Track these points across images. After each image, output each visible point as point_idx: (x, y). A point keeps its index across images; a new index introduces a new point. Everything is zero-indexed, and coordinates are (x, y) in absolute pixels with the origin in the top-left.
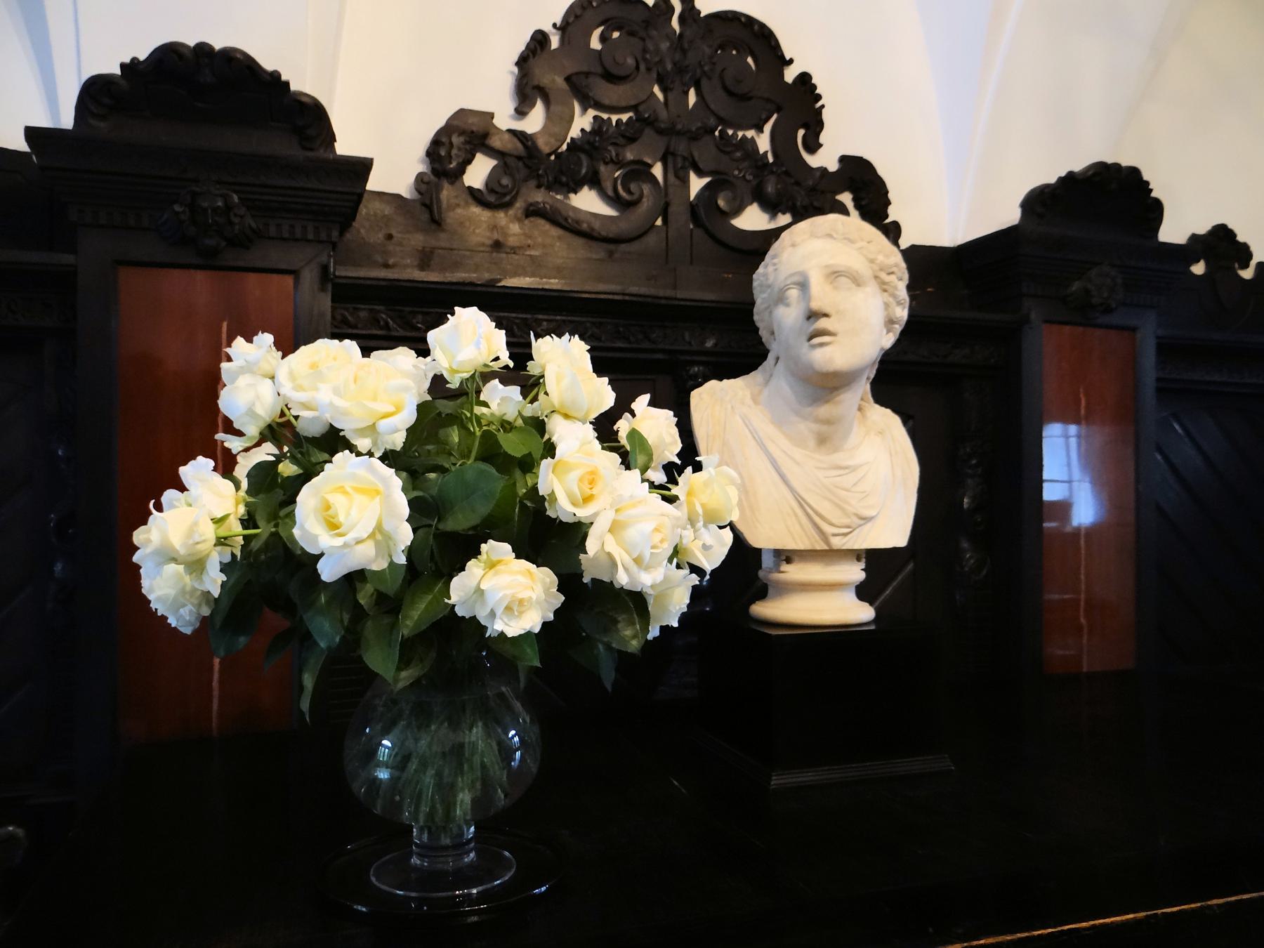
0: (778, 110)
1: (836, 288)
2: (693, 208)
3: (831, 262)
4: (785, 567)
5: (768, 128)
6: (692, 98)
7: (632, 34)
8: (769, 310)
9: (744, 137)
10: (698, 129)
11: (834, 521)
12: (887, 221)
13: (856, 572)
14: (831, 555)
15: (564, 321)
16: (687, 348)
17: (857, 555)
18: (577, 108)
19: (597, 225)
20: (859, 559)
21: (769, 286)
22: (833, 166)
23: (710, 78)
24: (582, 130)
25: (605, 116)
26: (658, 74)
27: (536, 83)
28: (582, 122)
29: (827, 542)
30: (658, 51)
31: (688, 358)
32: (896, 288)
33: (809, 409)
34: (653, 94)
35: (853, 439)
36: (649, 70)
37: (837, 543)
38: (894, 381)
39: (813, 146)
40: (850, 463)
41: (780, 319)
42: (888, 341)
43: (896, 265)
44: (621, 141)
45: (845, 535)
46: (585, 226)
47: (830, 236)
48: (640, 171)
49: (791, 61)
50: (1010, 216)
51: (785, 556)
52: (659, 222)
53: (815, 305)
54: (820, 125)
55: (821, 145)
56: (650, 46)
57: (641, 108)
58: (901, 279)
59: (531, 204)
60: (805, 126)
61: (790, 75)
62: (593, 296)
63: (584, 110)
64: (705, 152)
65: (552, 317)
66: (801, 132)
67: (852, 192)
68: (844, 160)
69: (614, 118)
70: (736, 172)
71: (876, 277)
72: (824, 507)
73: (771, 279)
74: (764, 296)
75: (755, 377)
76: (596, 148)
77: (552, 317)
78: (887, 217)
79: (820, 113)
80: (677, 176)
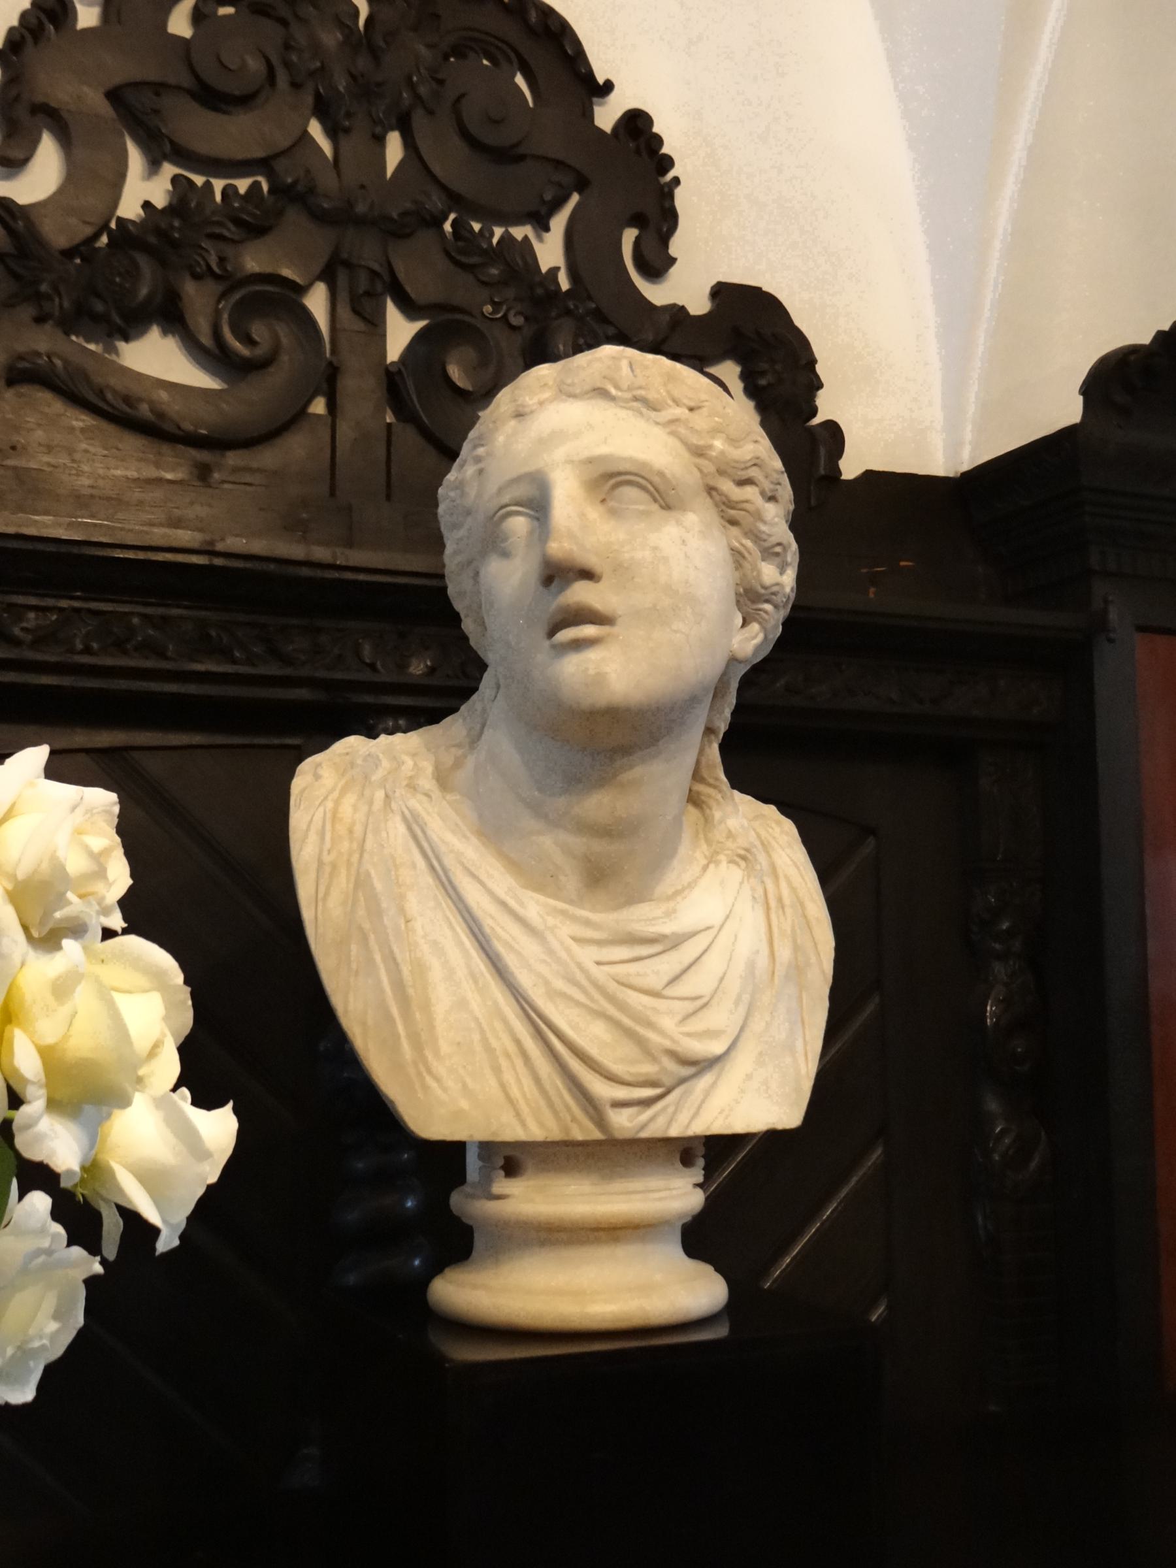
0: (582, 185)
1: (613, 513)
2: (393, 382)
3: (603, 450)
4: (502, 1185)
5: (559, 223)
6: (394, 150)
7: (261, 11)
8: (473, 567)
9: (507, 239)
10: (404, 214)
11: (618, 1069)
12: (816, 421)
13: (680, 1194)
14: (612, 1155)
15: (77, 610)
16: (367, 676)
17: (685, 1151)
18: (135, 159)
19: (174, 407)
20: (687, 1160)
21: (468, 512)
22: (699, 305)
23: (431, 112)
24: (147, 205)
25: (199, 180)
26: (318, 97)
27: (40, 99)
28: (143, 189)
29: (600, 1121)
30: (316, 48)
31: (369, 699)
32: (758, 516)
33: (561, 802)
34: (305, 136)
35: (679, 872)
36: (296, 85)
37: (624, 1122)
38: (777, 733)
39: (656, 265)
40: (667, 928)
41: (497, 590)
42: (750, 641)
43: (757, 463)
44: (230, 231)
45: (647, 1103)
46: (144, 410)
47: (601, 393)
48: (283, 298)
49: (608, 87)
50: (1066, 409)
51: (510, 1159)
52: (319, 407)
53: (558, 547)
54: (669, 219)
55: (673, 261)
56: (300, 36)
57: (280, 165)
58: (772, 499)
59: (21, 358)
60: (638, 220)
61: (606, 116)
62: (141, 556)
63: (154, 165)
64: (421, 267)
65: (50, 602)
66: (629, 236)
67: (740, 359)
68: (720, 291)
69: (218, 185)
70: (488, 309)
71: (711, 490)
72: (593, 1036)
73: (472, 492)
74: (462, 533)
75: (454, 727)
76: (175, 245)
77: (50, 602)
78: (814, 412)
79: (671, 196)
80: (356, 312)
